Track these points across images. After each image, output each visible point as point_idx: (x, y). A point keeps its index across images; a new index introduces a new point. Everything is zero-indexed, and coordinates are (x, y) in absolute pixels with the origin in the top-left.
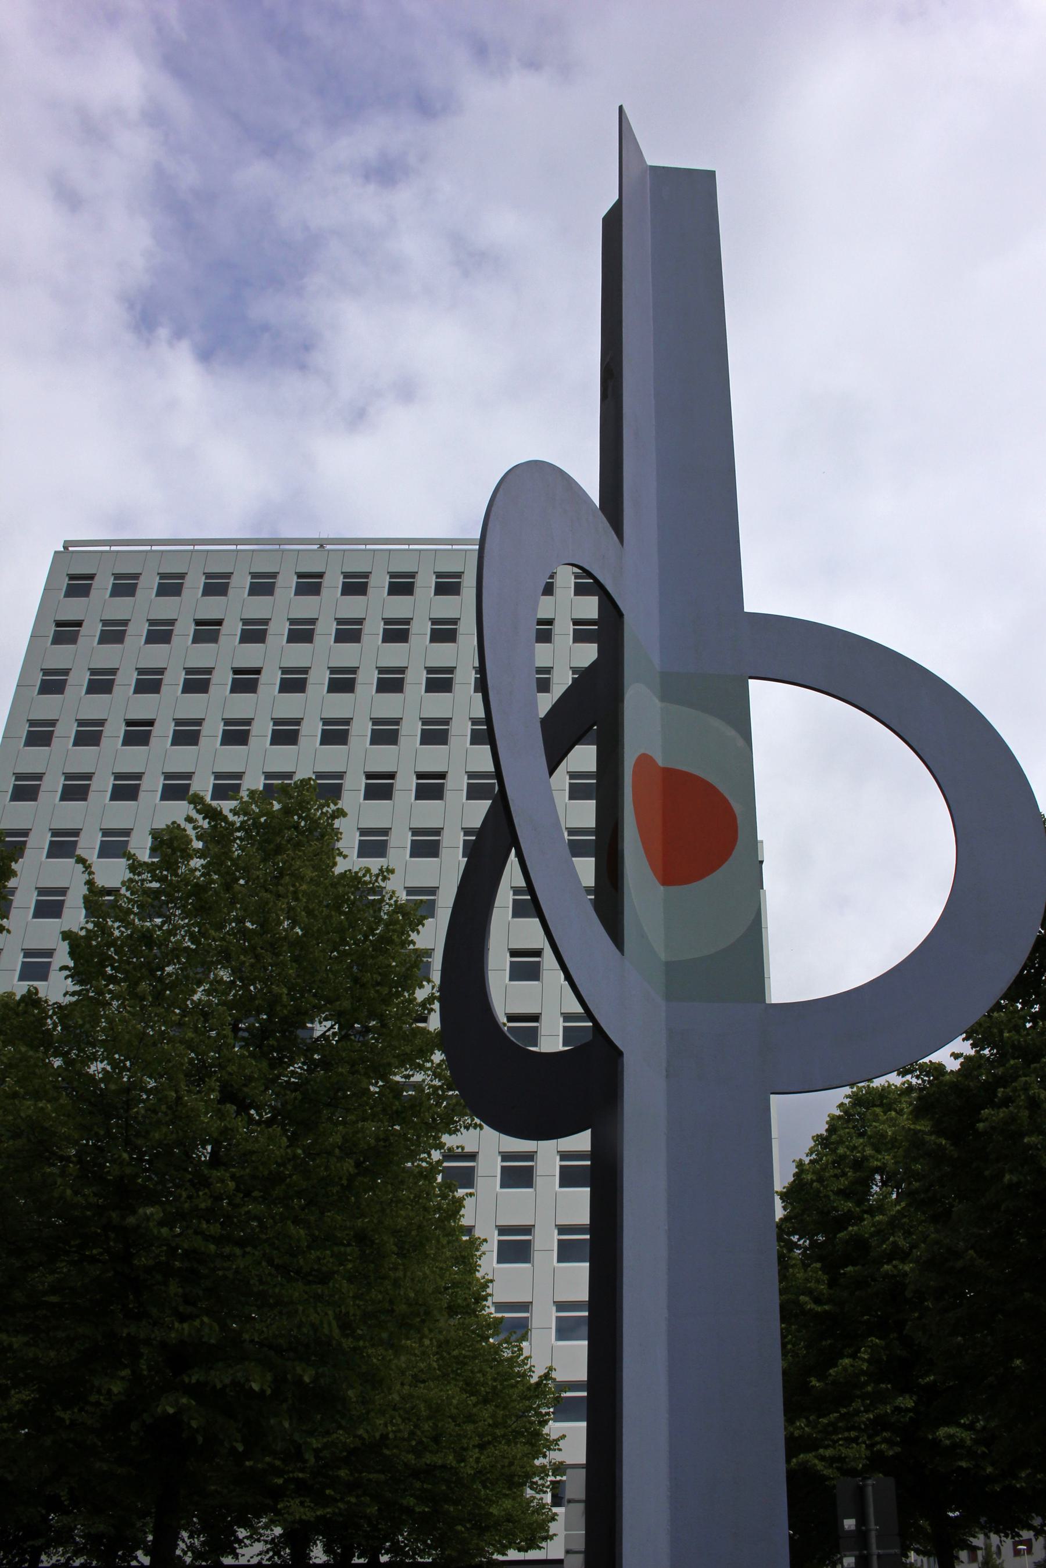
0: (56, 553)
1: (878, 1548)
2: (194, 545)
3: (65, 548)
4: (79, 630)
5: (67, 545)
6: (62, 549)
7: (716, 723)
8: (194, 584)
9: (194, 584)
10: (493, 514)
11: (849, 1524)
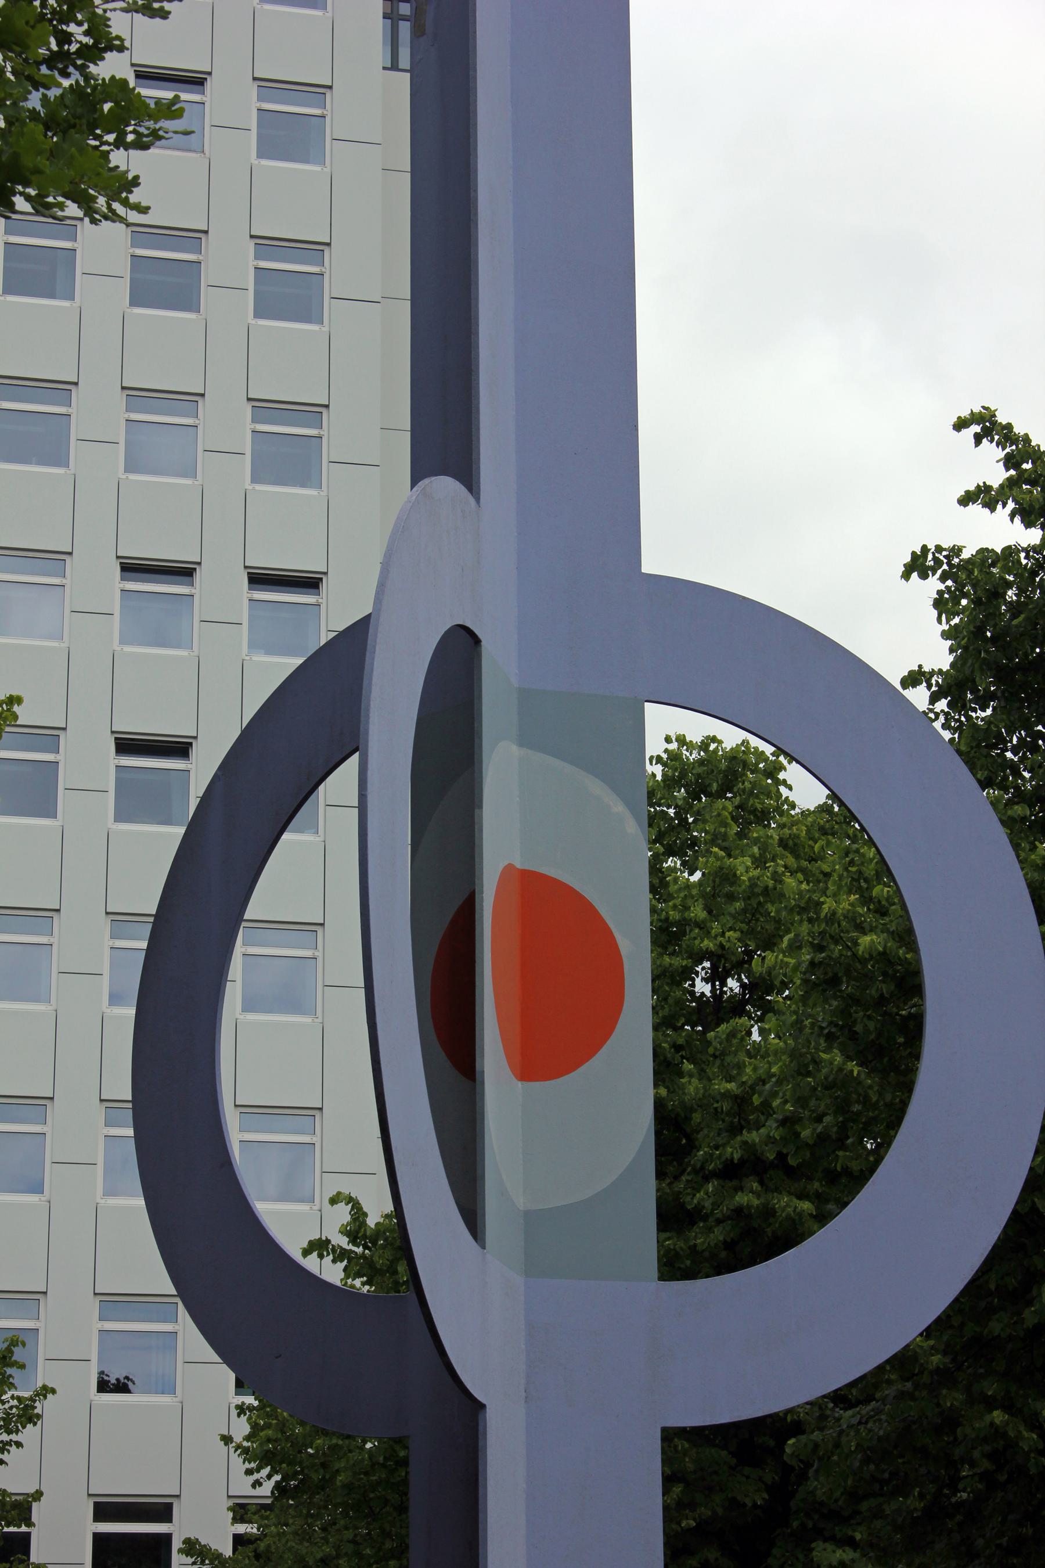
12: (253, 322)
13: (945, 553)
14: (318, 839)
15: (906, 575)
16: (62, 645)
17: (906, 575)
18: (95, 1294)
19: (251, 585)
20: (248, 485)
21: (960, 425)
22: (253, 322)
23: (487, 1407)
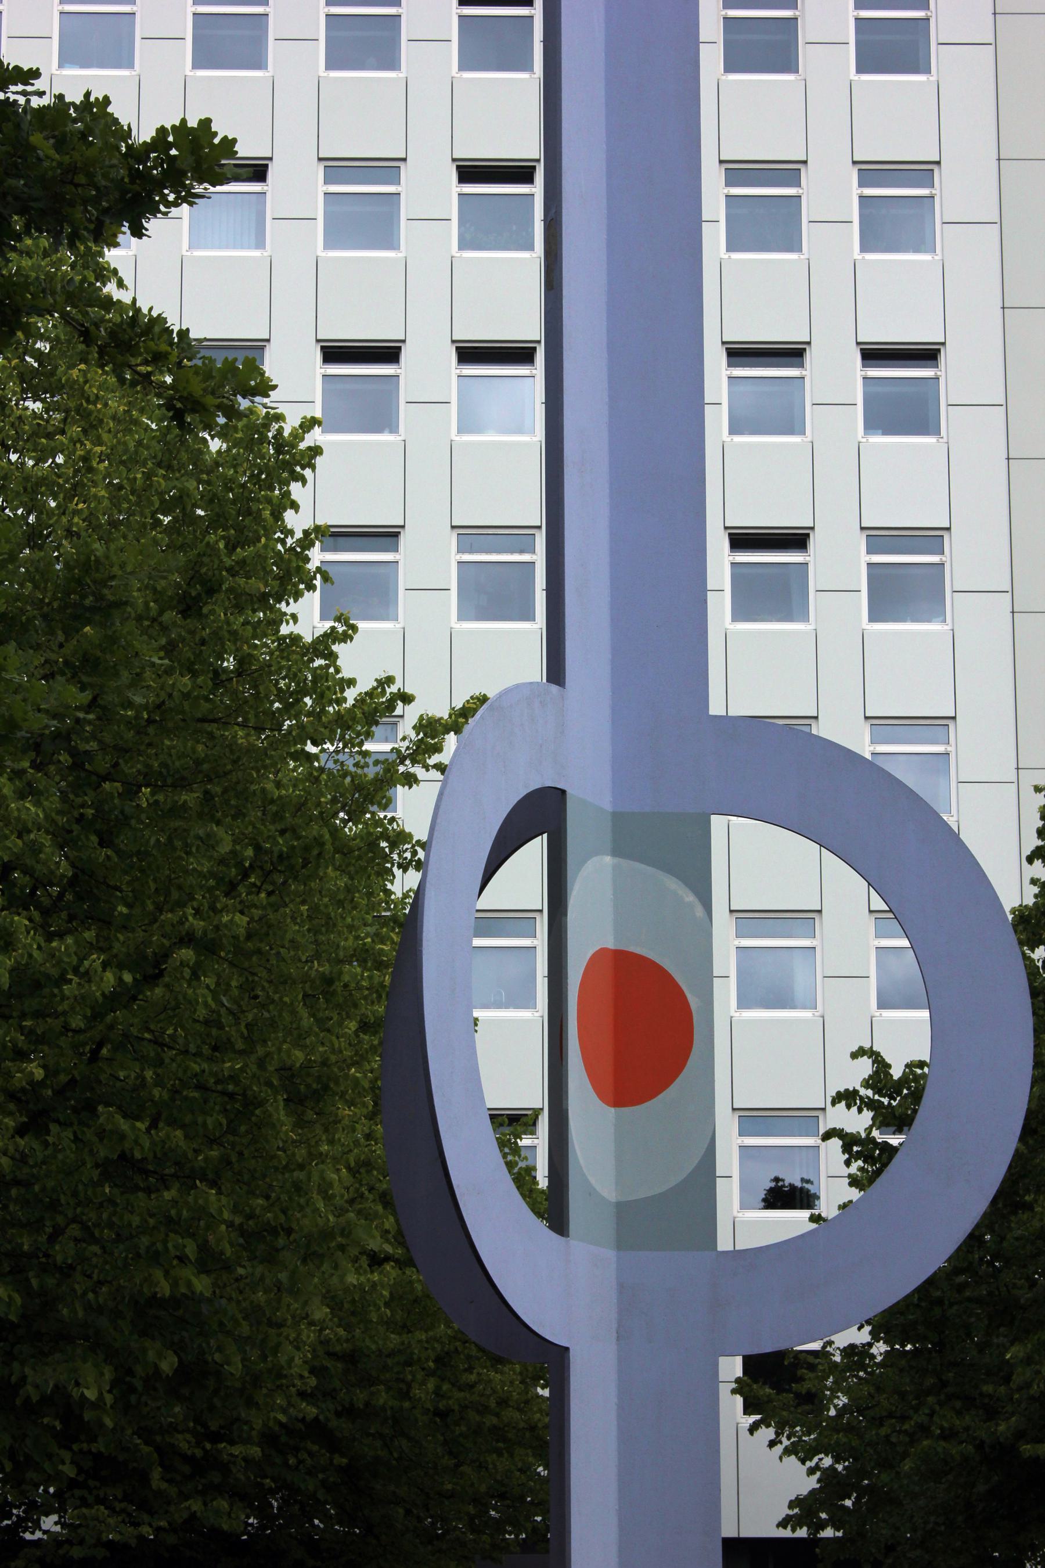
7: (672, 884)
12: (856, 78)
14: (946, 627)
16: (535, 439)
18: (734, 1109)
19: (734, 359)
20: (321, 252)
22: (856, 78)
23: (571, 1350)
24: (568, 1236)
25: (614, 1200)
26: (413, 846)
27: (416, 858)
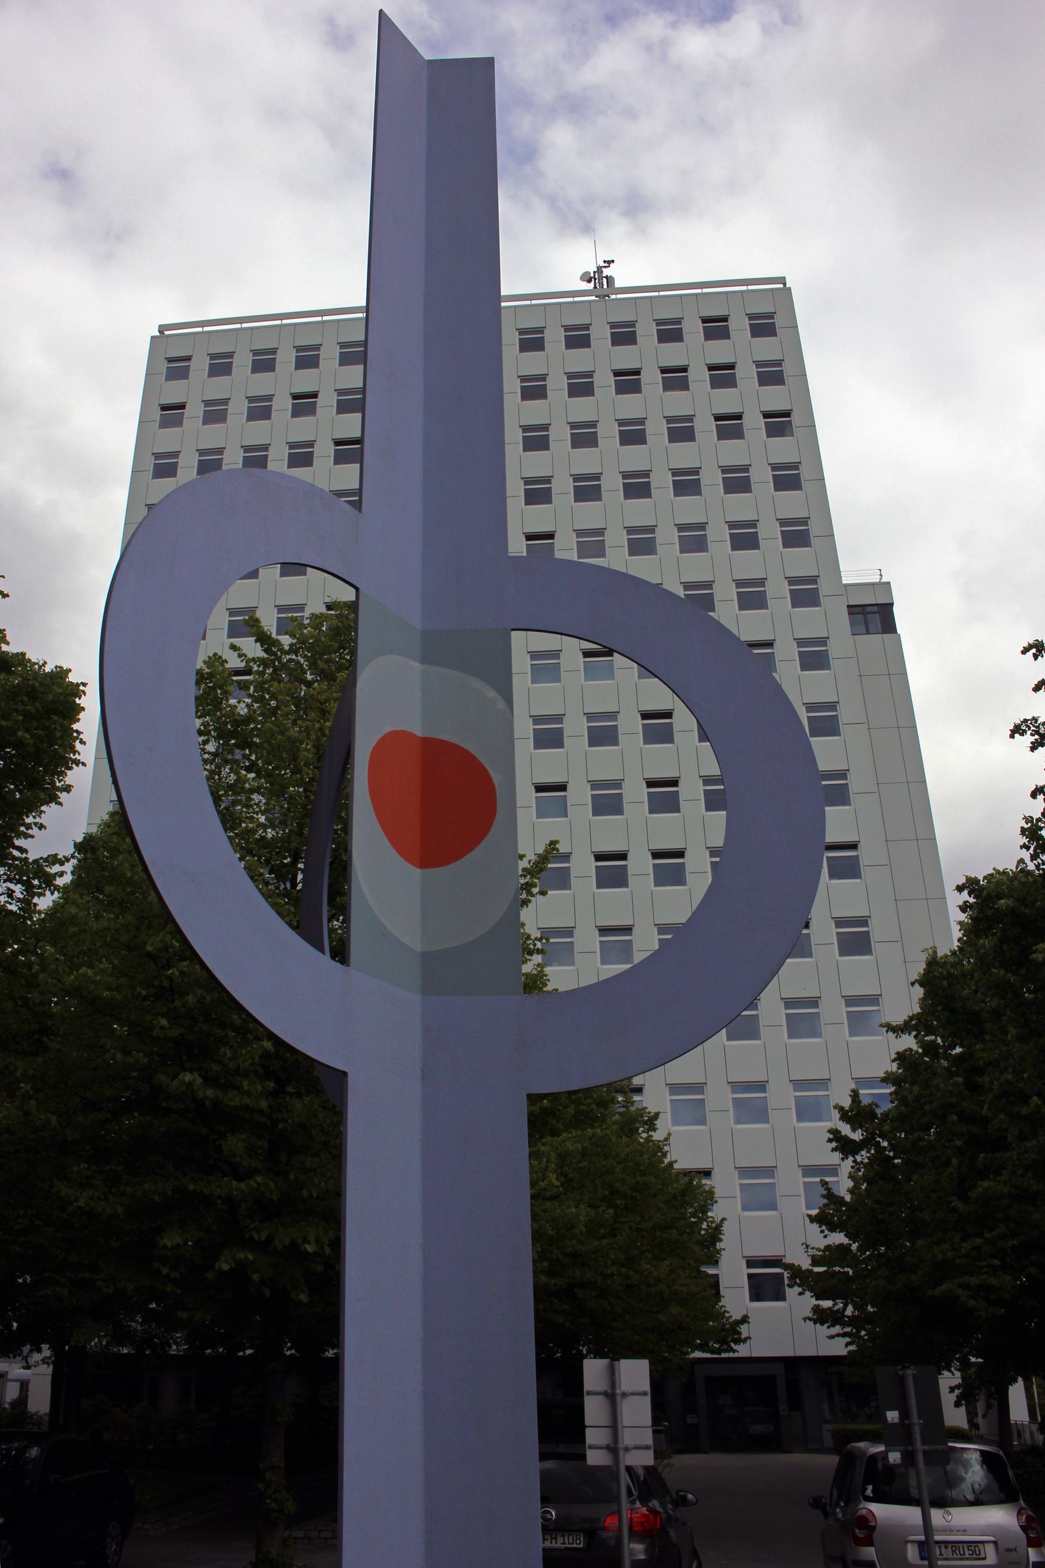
0: (153, 338)
1: (923, 1444)
2: (282, 320)
3: (161, 332)
4: (184, 412)
5: (162, 329)
6: (158, 334)
7: (476, 684)
8: (286, 358)
9: (286, 358)
10: (115, 586)
11: (893, 1416)
13: (1029, 722)
15: (1012, 736)
17: (1012, 736)
21: (1025, 651)
23: (349, 1075)
24: (348, 965)
25: (418, 946)
26: (534, 941)
27: (536, 947)
